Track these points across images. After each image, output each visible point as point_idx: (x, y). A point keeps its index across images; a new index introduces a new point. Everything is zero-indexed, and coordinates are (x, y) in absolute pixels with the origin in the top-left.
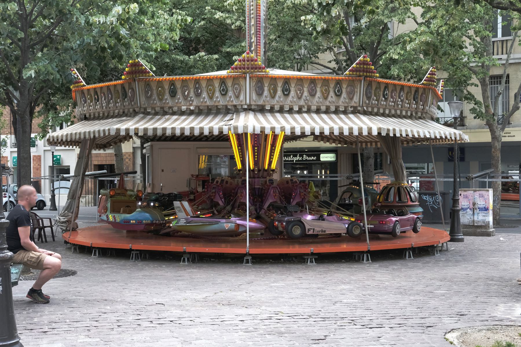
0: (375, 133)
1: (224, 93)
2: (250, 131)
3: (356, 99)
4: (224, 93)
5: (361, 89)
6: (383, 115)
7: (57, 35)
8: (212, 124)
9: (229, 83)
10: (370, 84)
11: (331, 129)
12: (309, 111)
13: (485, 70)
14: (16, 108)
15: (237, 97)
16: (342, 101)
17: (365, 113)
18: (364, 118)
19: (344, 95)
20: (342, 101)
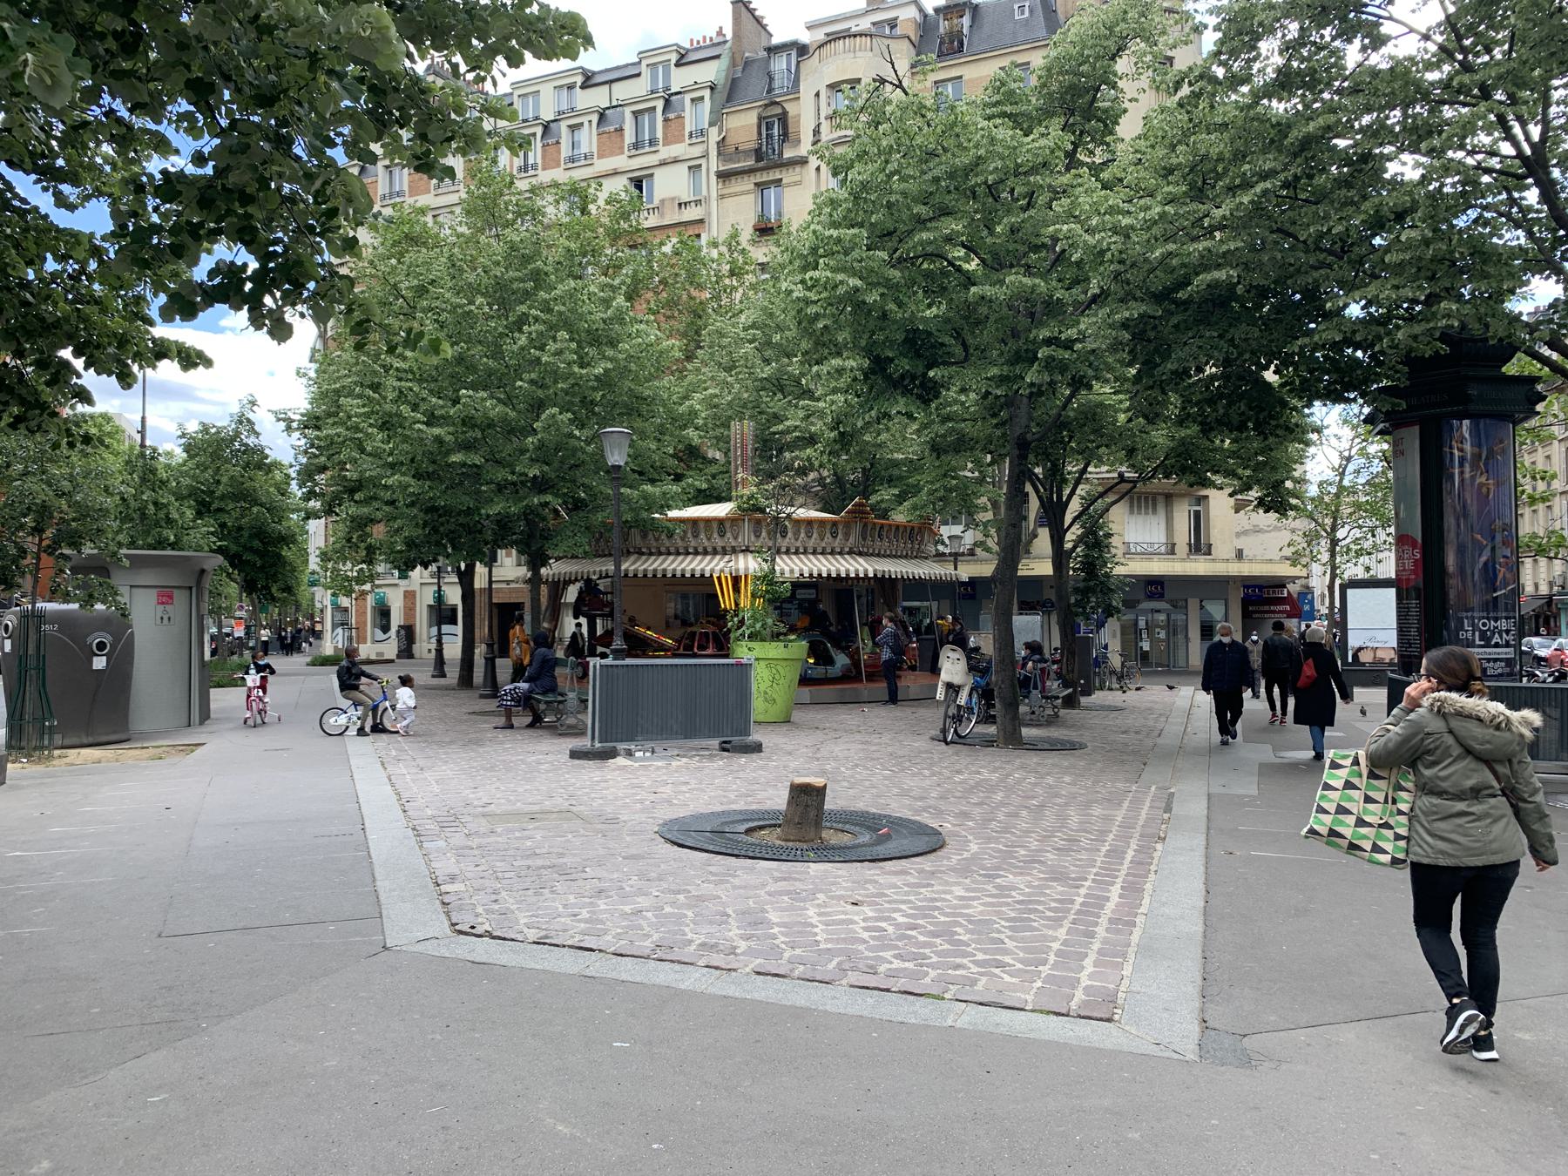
0: (871, 575)
1: (722, 534)
2: (751, 571)
3: (852, 540)
4: (722, 534)
5: (856, 530)
6: (878, 555)
7: (495, 161)
8: (722, 564)
9: (728, 525)
10: (865, 525)
11: (847, 571)
12: (805, 553)
13: (434, 538)
14: (66, 353)
15: (736, 538)
16: (837, 544)
17: (860, 554)
18: (861, 560)
19: (840, 536)
20: (811, 544)
